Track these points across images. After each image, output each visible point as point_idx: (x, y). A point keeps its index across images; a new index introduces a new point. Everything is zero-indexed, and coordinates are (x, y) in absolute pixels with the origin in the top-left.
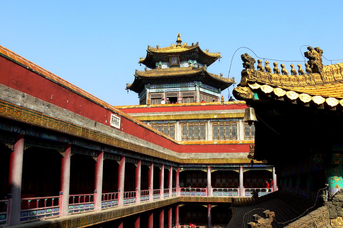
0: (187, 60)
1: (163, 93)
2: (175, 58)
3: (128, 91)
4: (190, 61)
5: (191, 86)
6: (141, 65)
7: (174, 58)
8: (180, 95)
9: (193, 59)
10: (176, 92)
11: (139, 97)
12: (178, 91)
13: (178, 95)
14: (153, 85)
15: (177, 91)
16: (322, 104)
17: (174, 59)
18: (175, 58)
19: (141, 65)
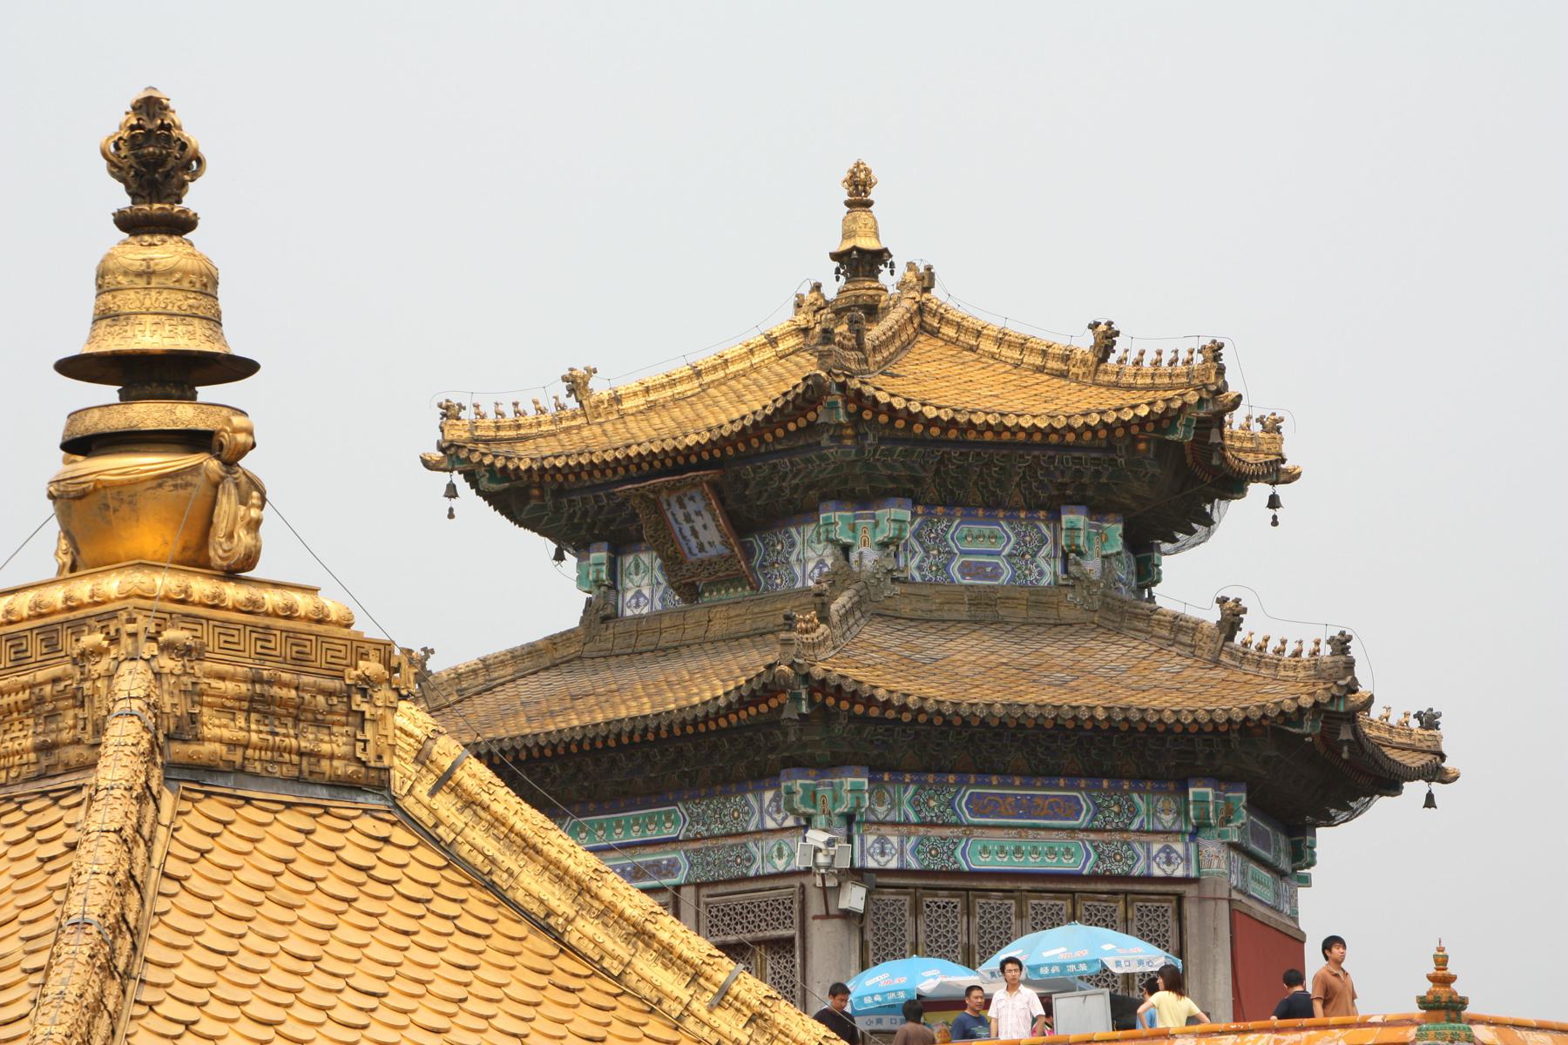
2: (691, 507)
4: (837, 520)
5: (770, 824)
12: (677, 888)
17: (688, 519)
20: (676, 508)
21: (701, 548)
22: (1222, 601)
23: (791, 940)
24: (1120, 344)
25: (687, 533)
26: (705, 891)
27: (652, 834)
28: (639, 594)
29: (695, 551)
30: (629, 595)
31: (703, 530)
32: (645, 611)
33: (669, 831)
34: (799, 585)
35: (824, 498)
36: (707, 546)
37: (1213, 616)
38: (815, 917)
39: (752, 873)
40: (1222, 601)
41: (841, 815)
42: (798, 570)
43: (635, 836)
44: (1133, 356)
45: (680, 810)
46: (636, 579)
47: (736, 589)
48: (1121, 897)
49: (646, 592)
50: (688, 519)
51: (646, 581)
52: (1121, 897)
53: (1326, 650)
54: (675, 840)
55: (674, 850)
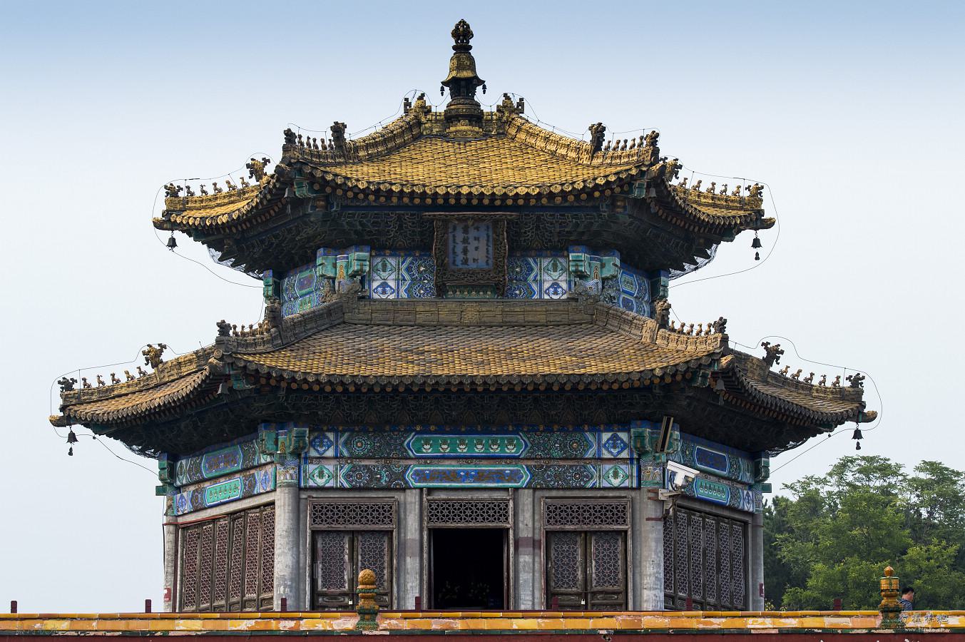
0: (558, 249)
1: (399, 496)
2: (473, 233)
3: (72, 438)
4: (579, 257)
5: (606, 455)
6: (172, 243)
7: (466, 230)
8: (527, 520)
9: (597, 248)
10: (497, 495)
11: (160, 491)
12: (516, 489)
13: (515, 515)
14: (331, 436)
15: (506, 489)
16: (474, 70)
17: (465, 241)
18: (473, 233)
19: (172, 243)
20: (460, 236)
21: (465, 262)
22: (765, 345)
23: (626, 532)
24: (608, 136)
25: (459, 249)
26: (538, 494)
27: (495, 450)
28: (384, 285)
29: (459, 262)
30: (375, 285)
31: (476, 250)
32: (392, 297)
33: (511, 450)
34: (536, 297)
35: (577, 243)
36: (470, 261)
37: (761, 354)
38: (648, 519)
39: (589, 485)
40: (765, 345)
41: (291, 453)
42: (535, 287)
43: (479, 450)
44: (613, 145)
45: (521, 439)
46: (383, 274)
47: (478, 292)
48: (579, 540)
49: (392, 284)
50: (465, 241)
51: (393, 276)
52: (579, 540)
53: (847, 384)
54: (517, 458)
55: (516, 465)
